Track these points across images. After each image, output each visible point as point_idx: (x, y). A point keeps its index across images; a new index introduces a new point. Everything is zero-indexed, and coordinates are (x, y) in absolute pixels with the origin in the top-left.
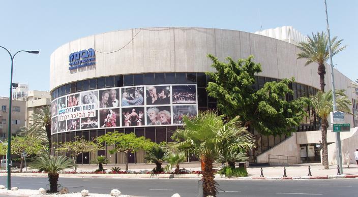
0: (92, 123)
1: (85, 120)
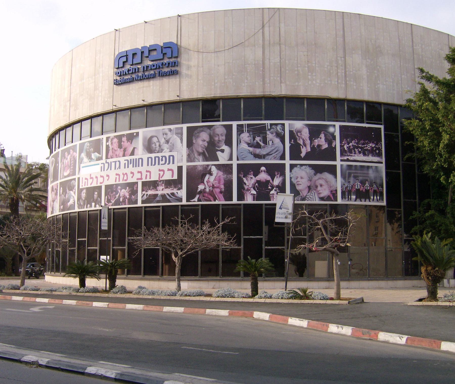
0: (168, 191)
1: (147, 185)
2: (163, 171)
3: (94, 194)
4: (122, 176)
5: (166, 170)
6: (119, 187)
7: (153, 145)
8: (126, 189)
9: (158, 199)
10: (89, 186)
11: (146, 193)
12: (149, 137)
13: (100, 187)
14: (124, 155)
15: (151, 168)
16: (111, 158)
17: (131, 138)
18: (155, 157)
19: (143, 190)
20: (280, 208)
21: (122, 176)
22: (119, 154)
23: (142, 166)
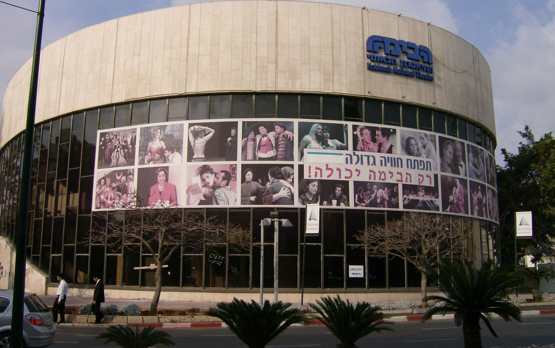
0: (427, 198)
1: (409, 189)
2: (422, 176)
3: (335, 189)
4: (378, 175)
5: (425, 176)
6: (375, 186)
7: (412, 147)
8: (384, 189)
9: (419, 205)
10: (325, 178)
11: (407, 197)
12: (406, 138)
13: (347, 183)
14: (379, 151)
15: (410, 171)
16: (362, 150)
17: (387, 133)
18: (415, 160)
19: (404, 194)
20: (521, 225)
21: (378, 175)
22: (373, 149)
23: (402, 167)
